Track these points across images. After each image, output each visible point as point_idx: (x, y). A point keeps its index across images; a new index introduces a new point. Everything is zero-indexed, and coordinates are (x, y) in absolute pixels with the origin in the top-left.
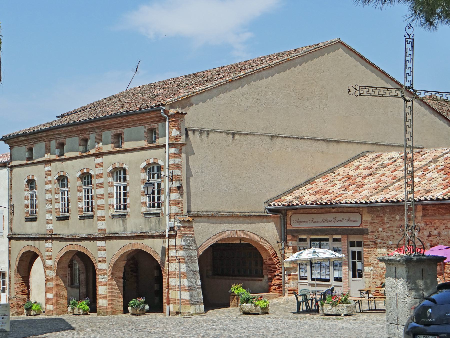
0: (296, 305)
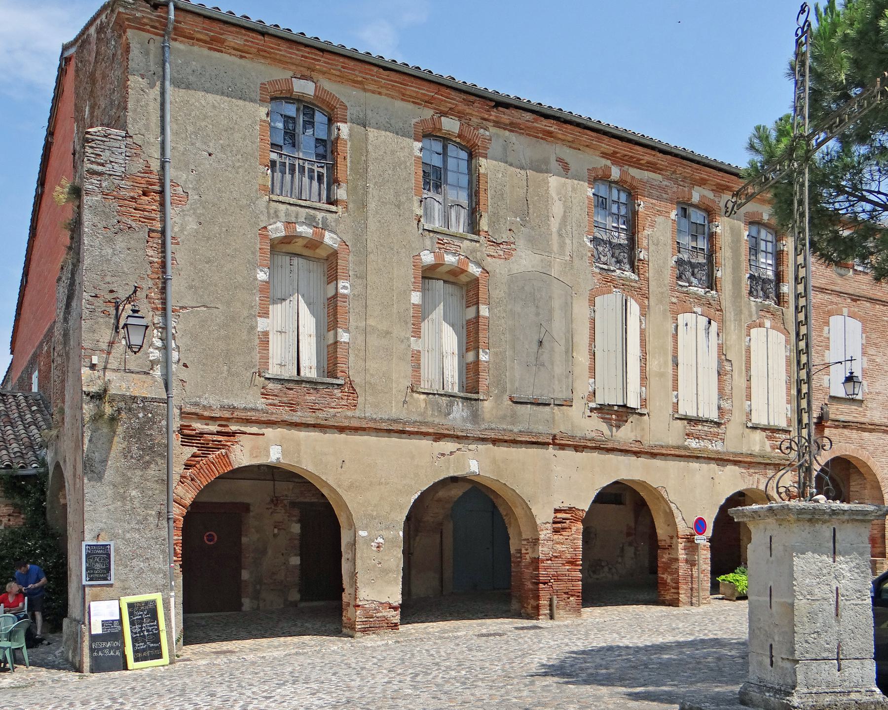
0: (391, 542)
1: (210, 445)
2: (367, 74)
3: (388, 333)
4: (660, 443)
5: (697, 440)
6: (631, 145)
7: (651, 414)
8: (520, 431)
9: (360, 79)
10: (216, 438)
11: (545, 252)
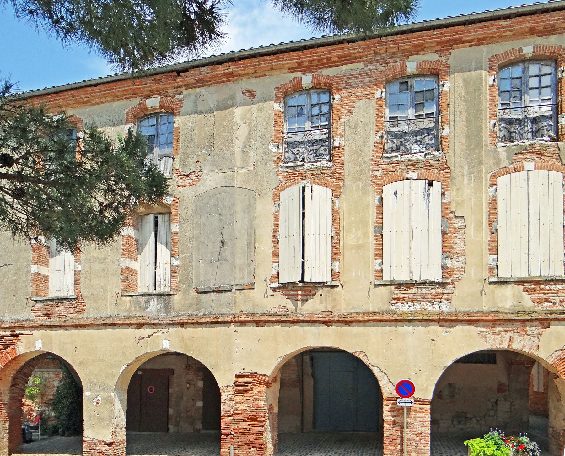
1: (8, 343)
2: (87, 94)
3: (105, 259)
4: (357, 311)
5: (410, 304)
6: (313, 50)
7: (344, 285)
8: (205, 315)
9: (86, 99)
10: (9, 338)
11: (228, 169)
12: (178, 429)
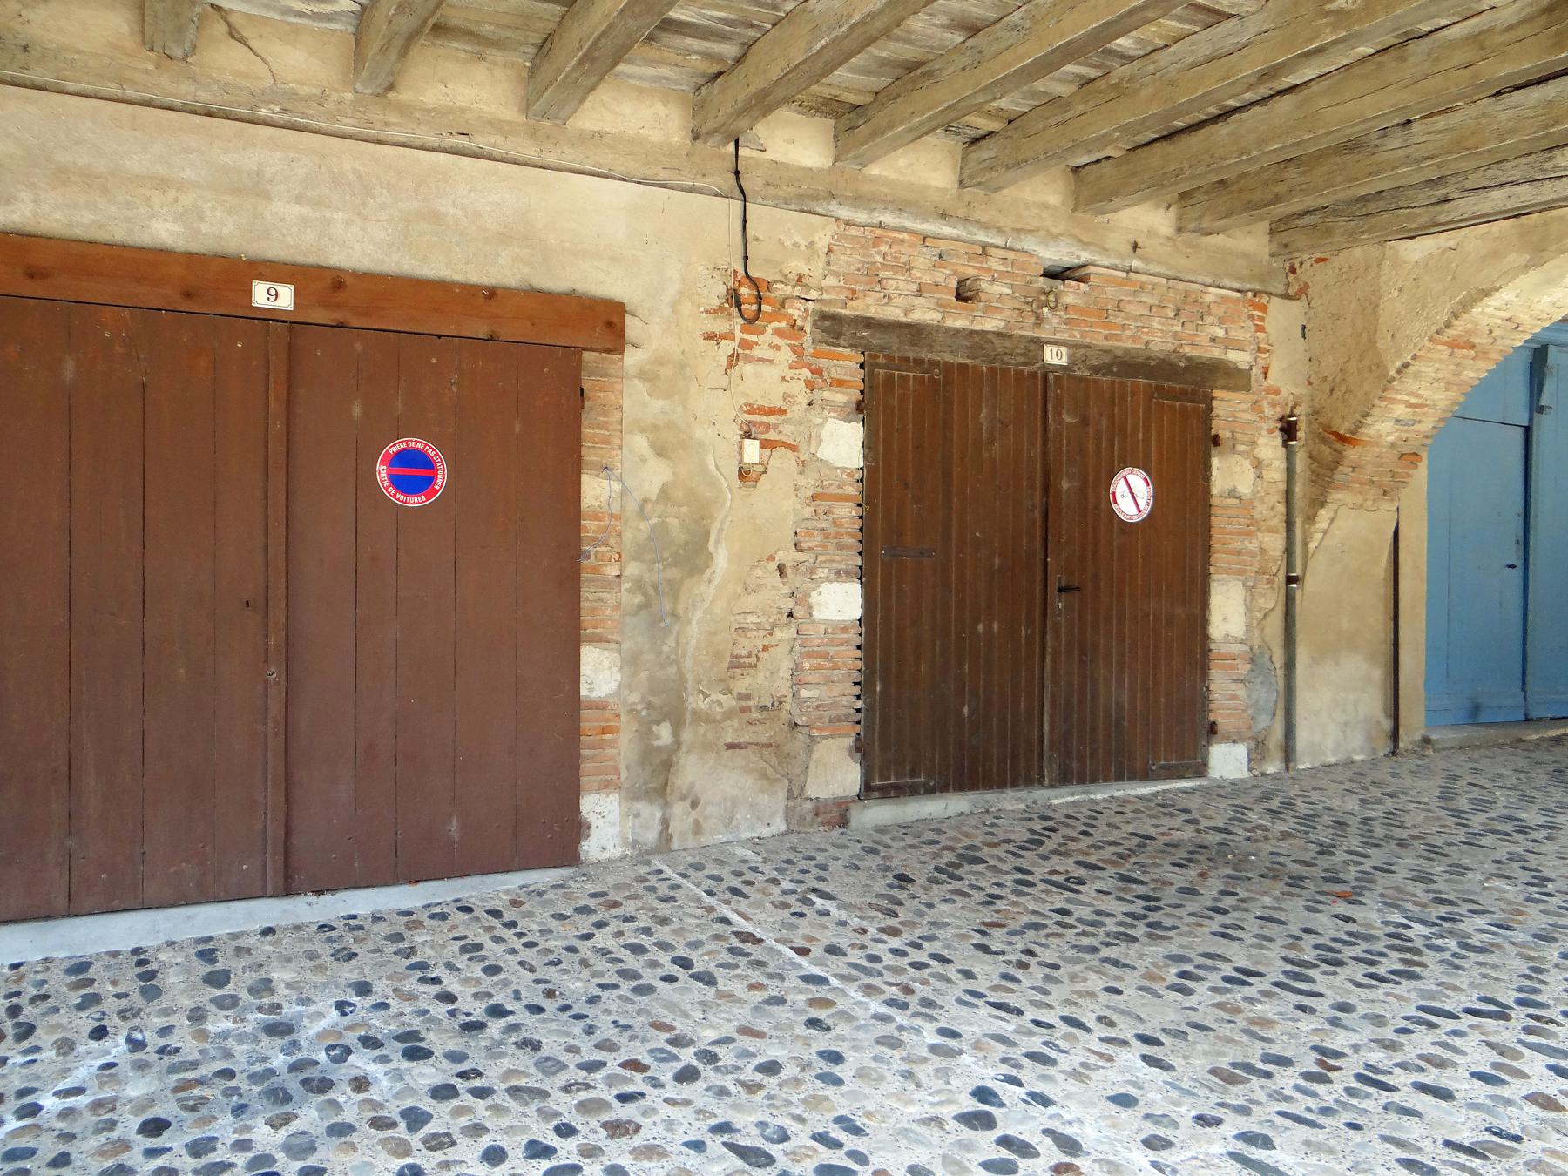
12: (665, 823)
